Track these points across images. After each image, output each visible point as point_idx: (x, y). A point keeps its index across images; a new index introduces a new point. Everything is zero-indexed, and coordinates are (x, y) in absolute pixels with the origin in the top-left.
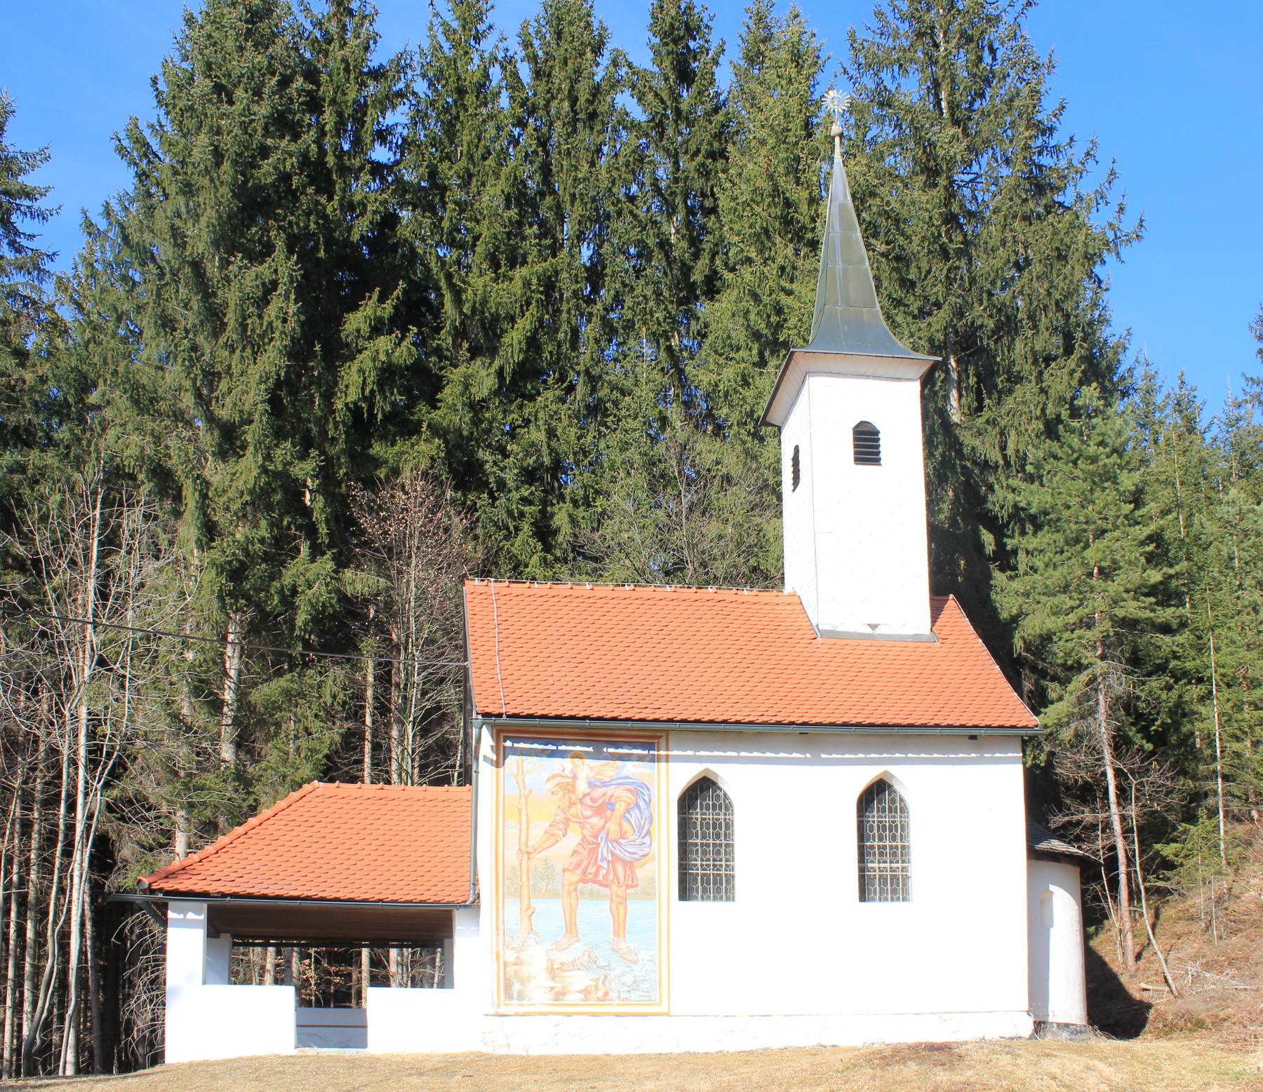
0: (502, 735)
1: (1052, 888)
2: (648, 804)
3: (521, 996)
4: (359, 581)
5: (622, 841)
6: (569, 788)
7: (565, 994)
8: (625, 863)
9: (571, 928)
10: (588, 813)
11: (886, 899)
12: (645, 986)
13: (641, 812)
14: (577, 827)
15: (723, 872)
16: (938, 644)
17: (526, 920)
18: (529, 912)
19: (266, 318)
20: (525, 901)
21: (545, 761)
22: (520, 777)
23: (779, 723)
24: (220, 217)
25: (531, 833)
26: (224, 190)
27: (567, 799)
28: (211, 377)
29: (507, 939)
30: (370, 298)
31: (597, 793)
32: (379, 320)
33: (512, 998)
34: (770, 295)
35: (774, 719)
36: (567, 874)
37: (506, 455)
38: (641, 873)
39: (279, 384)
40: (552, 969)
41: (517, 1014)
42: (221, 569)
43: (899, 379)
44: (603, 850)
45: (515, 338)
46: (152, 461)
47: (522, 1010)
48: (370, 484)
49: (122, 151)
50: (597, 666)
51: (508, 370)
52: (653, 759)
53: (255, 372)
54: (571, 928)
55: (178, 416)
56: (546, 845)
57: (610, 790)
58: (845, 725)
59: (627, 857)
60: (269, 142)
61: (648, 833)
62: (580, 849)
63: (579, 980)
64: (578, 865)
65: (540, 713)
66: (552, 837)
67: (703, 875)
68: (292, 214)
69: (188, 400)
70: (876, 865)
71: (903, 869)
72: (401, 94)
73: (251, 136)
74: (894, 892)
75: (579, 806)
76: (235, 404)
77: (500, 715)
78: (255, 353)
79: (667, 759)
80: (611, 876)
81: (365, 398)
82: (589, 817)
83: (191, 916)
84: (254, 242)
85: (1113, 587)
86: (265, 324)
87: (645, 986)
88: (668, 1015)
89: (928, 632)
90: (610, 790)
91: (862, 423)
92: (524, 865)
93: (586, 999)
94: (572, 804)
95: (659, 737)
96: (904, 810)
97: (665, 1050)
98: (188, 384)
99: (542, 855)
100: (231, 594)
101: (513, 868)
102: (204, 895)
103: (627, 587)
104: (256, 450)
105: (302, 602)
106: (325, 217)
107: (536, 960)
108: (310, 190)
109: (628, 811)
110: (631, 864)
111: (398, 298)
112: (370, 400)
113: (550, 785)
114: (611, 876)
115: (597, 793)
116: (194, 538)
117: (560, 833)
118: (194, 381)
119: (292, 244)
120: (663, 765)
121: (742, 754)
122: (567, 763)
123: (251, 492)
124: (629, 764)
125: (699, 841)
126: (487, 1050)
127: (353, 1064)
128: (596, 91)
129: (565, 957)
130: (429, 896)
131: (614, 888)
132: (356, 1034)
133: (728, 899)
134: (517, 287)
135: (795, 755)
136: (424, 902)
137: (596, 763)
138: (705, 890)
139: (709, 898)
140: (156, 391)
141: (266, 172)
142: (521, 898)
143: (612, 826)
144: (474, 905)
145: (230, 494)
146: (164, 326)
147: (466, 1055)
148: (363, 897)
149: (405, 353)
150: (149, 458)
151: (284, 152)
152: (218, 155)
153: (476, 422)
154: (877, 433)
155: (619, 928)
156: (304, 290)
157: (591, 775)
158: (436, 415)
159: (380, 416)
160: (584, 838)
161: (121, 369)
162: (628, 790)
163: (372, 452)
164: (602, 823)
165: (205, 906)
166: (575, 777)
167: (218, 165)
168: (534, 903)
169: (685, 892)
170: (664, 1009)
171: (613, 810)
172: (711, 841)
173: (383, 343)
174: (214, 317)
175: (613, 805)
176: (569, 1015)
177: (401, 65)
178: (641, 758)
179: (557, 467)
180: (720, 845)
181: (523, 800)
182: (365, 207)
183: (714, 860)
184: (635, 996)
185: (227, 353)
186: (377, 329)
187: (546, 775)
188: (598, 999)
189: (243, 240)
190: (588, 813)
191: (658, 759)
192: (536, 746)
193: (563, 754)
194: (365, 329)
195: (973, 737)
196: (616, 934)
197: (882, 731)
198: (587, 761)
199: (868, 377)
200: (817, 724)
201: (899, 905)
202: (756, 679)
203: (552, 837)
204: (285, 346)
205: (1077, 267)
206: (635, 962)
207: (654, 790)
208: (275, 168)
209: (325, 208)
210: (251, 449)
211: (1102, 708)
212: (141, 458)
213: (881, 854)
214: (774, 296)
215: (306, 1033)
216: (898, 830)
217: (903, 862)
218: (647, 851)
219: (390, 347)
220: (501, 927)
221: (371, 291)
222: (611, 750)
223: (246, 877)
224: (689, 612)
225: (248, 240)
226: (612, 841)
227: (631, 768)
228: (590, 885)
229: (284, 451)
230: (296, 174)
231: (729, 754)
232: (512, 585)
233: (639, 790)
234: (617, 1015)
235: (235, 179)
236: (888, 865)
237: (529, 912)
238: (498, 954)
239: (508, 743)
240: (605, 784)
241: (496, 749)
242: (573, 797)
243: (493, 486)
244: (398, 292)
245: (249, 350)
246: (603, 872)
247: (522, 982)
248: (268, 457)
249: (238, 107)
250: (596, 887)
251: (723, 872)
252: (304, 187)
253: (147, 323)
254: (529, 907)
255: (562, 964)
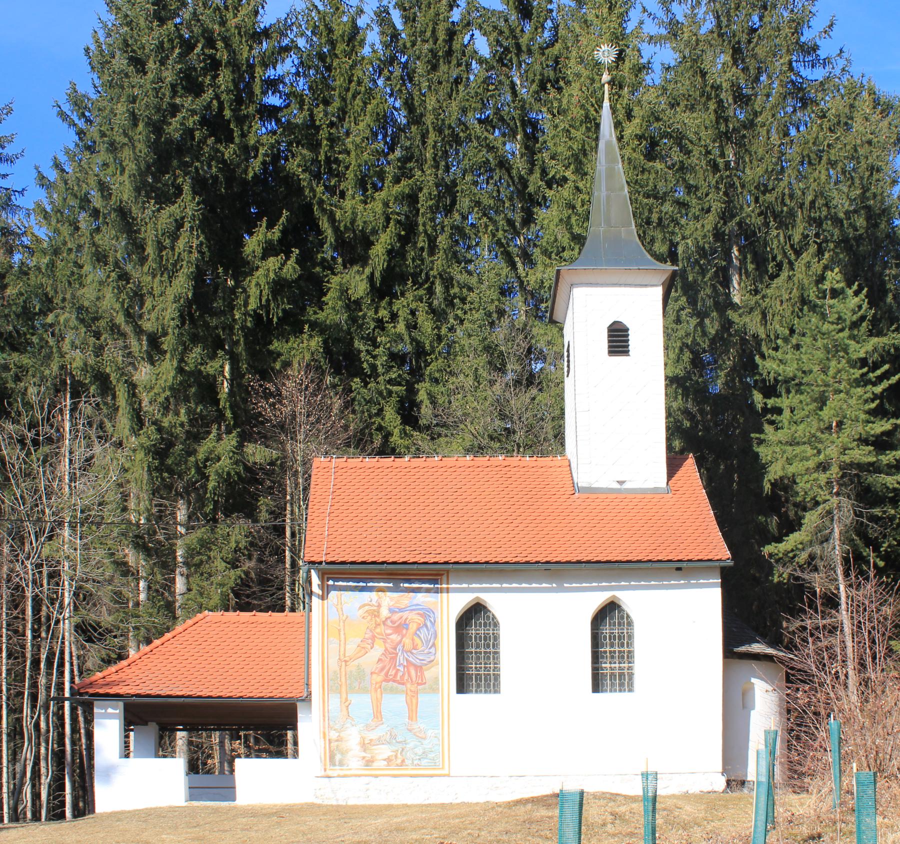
0: (326, 576)
1: (753, 680)
2: (433, 624)
3: (341, 764)
4: (257, 453)
5: (414, 651)
6: (375, 613)
7: (373, 762)
8: (416, 667)
9: (378, 714)
10: (389, 631)
11: (615, 691)
12: (431, 756)
13: (428, 630)
14: (381, 642)
15: (492, 672)
16: (670, 495)
17: (345, 709)
18: (347, 704)
19: (177, 250)
20: (344, 696)
21: (357, 594)
22: (339, 607)
23: (527, 562)
24: (140, 168)
25: (348, 647)
26: (140, 146)
27: (373, 622)
28: (139, 297)
29: (331, 723)
30: (261, 226)
31: (396, 617)
32: (269, 243)
33: (334, 765)
34: (583, 205)
35: (525, 559)
36: (374, 676)
37: (375, 345)
38: (428, 674)
39: (189, 303)
40: (364, 744)
41: (339, 776)
42: (148, 451)
43: (646, 286)
44: (400, 658)
45: (379, 251)
46: (94, 369)
47: (342, 773)
48: (265, 374)
49: (63, 115)
50: (401, 522)
51: (377, 275)
52: (437, 591)
53: (171, 293)
54: (378, 714)
55: (114, 329)
56: (360, 655)
57: (405, 615)
58: (579, 562)
59: (418, 662)
60: (178, 101)
61: (434, 645)
62: (383, 658)
63: (384, 751)
64: (382, 669)
65: (350, 560)
66: (363, 650)
67: (476, 675)
68: (198, 161)
69: (120, 319)
70: (608, 665)
71: (629, 668)
72: (286, 49)
73: (161, 99)
74: (621, 685)
75: (382, 626)
76: (158, 319)
77: (321, 563)
78: (170, 277)
79: (448, 590)
80: (406, 677)
81: (261, 307)
83: (110, 710)
84: (168, 185)
85: (844, 438)
86: (177, 254)
87: (431, 756)
88: (448, 776)
89: (664, 485)
90: (405, 615)
91: (615, 323)
92: (343, 669)
93: (388, 765)
94: (377, 625)
95: (442, 575)
96: (630, 624)
97: (446, 800)
98: (117, 306)
99: (356, 662)
100: (156, 469)
101: (335, 672)
102: (117, 695)
103: (436, 458)
104: (172, 356)
105: (212, 471)
106: (224, 162)
107: (353, 738)
108: (212, 140)
109: (418, 629)
110: (421, 667)
111: (283, 224)
112: (267, 307)
113: (361, 612)
114: (406, 677)
115: (396, 617)
116: (128, 427)
117: (369, 647)
118: (123, 304)
119: (201, 186)
120: (445, 595)
121: (504, 585)
122: (374, 595)
123: (171, 388)
124: (420, 595)
125: (473, 650)
126: (318, 801)
127: (230, 809)
128: (451, 34)
129: (373, 735)
130: (277, 693)
131: (409, 685)
132: (228, 791)
133: (630, 690)
134: (378, 206)
135: (544, 585)
136: (272, 697)
137: (395, 595)
138: (478, 686)
139: (481, 692)
140: (97, 312)
141: (174, 128)
142: (340, 693)
143: (407, 641)
144: (308, 699)
145: (156, 391)
146: (98, 260)
147: (302, 805)
148: (228, 695)
149: (291, 269)
150: (91, 367)
151: (188, 110)
152: (134, 119)
153: (353, 320)
154: (627, 330)
155: (413, 714)
156: (206, 224)
157: (391, 604)
158: (321, 316)
159: (275, 320)
160: (386, 650)
161: (68, 296)
163: (272, 347)
164: (399, 638)
165: (121, 704)
166: (379, 606)
167: (136, 125)
168: (350, 697)
169: (462, 686)
170: (446, 772)
171: (407, 629)
172: (483, 650)
173: (273, 263)
174: (138, 247)
175: (408, 625)
176: (376, 776)
177: (283, 28)
178: (428, 591)
179: (420, 352)
180: (490, 653)
181: (342, 624)
182: (257, 151)
183: (485, 664)
184: (424, 762)
185: (150, 278)
186: (269, 250)
187: (358, 605)
188: (397, 765)
189: (159, 185)
190: (389, 631)
191: (441, 591)
192: (351, 584)
193: (371, 589)
194: (259, 251)
195: (679, 569)
196: (410, 718)
197: (607, 565)
198: (388, 594)
199: (620, 285)
200: (557, 562)
201: (625, 695)
202: (520, 528)
203: (363, 650)
204: (192, 273)
205: (823, 171)
206: (424, 739)
207: (438, 614)
208: (181, 124)
209: (223, 155)
210: (168, 356)
211: (836, 534)
212: (85, 368)
213: (612, 657)
214: (586, 207)
215: (194, 792)
216: (626, 639)
217: (629, 663)
218: (432, 658)
219: (278, 265)
220: (326, 714)
221: (261, 220)
222: (406, 585)
223: (209, 678)
224: (480, 476)
225: (164, 185)
227: (421, 598)
228: (391, 683)
229: (196, 353)
230: (198, 129)
231: (494, 585)
232: (349, 460)
233: (427, 614)
234: (411, 776)
235: (148, 137)
236: (617, 665)
237: (347, 704)
238: (324, 734)
239: (331, 582)
240: (401, 610)
241: (322, 587)
242: (378, 620)
243: (368, 371)
244: (283, 219)
245: (166, 275)
246: (400, 674)
247: (342, 754)
248: (181, 360)
249: (150, 76)
250: (395, 685)
251: (492, 672)
252: (206, 138)
253: (85, 257)
254: (346, 700)
255: (371, 740)
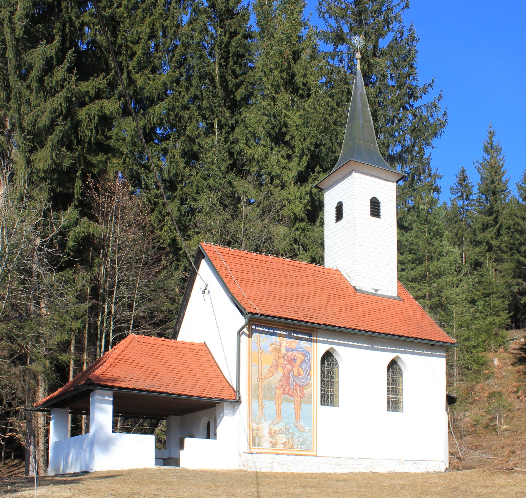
5: (299, 377)
7: (276, 445)
56: (269, 375)
82: (286, 365)
117: (275, 371)
162: (301, 354)
164: (291, 368)
181: (260, 354)
220: (251, 412)
226: (295, 377)
237: (262, 406)
242: (280, 355)
255: (275, 431)
